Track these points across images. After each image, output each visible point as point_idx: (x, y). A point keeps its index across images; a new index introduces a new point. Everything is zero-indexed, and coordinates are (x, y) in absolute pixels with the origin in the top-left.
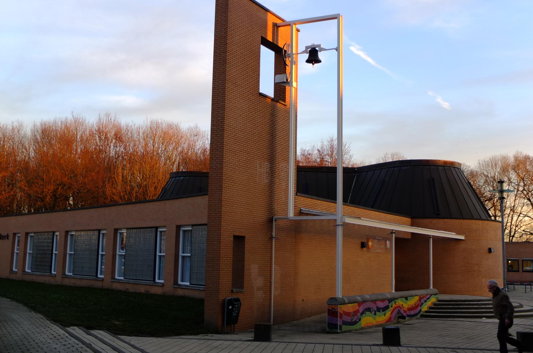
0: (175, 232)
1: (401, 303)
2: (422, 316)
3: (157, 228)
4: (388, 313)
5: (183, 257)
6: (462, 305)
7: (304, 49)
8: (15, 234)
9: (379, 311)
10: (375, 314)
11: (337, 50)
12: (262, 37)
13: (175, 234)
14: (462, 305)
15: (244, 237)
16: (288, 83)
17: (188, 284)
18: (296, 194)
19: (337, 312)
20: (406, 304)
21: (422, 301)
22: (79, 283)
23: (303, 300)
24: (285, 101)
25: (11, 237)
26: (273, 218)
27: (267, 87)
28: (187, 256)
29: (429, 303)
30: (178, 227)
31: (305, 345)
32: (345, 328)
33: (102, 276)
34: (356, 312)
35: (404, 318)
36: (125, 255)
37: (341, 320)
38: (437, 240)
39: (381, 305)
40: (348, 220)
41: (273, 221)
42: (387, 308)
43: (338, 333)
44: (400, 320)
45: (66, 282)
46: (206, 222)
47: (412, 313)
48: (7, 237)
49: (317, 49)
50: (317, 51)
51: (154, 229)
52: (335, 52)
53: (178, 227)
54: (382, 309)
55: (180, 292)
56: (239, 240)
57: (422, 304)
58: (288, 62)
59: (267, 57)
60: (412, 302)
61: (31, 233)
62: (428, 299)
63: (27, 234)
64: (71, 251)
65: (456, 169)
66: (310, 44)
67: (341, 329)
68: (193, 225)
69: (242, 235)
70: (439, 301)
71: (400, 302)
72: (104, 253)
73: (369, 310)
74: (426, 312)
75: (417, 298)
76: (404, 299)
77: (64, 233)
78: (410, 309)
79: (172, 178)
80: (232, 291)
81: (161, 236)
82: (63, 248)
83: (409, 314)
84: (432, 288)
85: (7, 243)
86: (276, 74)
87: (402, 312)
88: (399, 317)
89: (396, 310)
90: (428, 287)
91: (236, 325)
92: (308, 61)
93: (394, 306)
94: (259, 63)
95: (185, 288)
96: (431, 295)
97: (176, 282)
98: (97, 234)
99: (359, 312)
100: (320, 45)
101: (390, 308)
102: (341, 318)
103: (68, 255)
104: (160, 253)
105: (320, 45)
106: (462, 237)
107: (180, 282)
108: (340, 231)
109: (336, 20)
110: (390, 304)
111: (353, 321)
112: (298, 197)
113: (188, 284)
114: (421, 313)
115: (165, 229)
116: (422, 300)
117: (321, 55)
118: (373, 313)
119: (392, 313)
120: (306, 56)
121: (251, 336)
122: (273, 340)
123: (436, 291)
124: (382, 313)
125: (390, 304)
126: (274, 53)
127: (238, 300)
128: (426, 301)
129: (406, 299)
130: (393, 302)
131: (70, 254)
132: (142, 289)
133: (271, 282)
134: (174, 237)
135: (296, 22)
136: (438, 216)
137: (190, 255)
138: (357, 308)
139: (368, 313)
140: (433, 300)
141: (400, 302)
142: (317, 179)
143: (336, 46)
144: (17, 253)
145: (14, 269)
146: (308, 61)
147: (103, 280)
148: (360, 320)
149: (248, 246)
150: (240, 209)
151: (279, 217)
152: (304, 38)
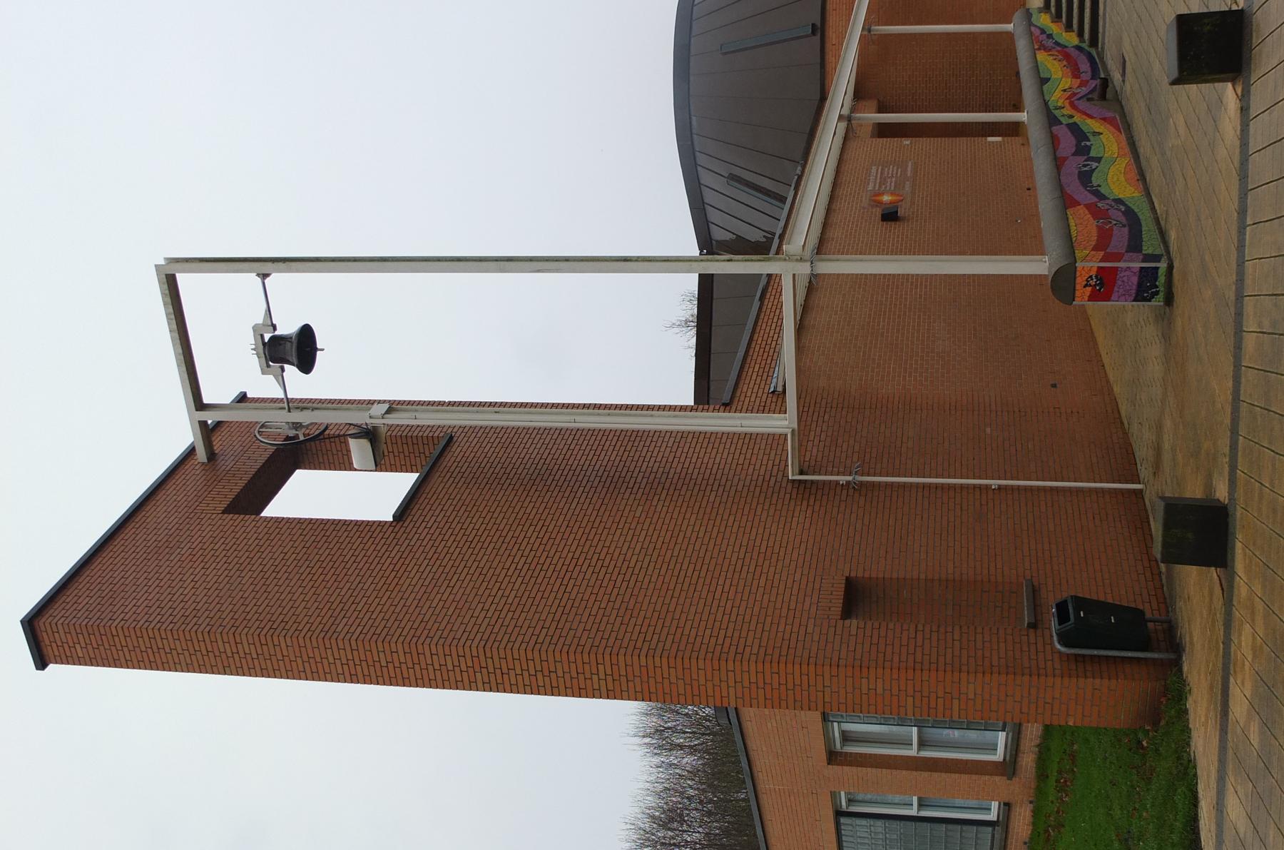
0: (846, 768)
1: (1058, 94)
3: (839, 814)
4: (1091, 125)
5: (922, 744)
7: (270, 379)
9: (1088, 148)
10: (1098, 160)
13: (854, 769)
15: (847, 579)
16: (370, 434)
18: (726, 405)
19: (1099, 268)
20: (1061, 81)
21: (1049, 43)
23: (1054, 386)
29: (1056, 29)
32: (1150, 244)
33: (995, 805)
35: (1105, 83)
37: (1127, 256)
39: (1068, 143)
42: (1075, 129)
43: (1170, 268)
44: (1109, 95)
47: (1085, 66)
49: (267, 337)
50: (273, 339)
51: (843, 820)
52: (278, 280)
55: (1028, 761)
57: (1057, 43)
59: (306, 496)
60: (1053, 66)
62: (1043, 31)
67: (1157, 258)
71: (1056, 97)
72: (915, 799)
73: (1085, 177)
74: (1080, 34)
75: (1041, 56)
76: (1045, 87)
77: (835, 769)
78: (1076, 73)
83: (1089, 74)
84: (1009, 27)
86: (351, 468)
87: (1084, 90)
88: (1103, 97)
89: (1083, 105)
90: (1010, 36)
91: (1148, 615)
94: (300, 521)
101: (1076, 119)
102: (1117, 257)
105: (255, 328)
107: (999, 756)
110: (1064, 121)
111: (1124, 221)
115: (843, 794)
116: (1042, 41)
117: (288, 327)
118: (1094, 165)
119: (1091, 117)
120: (291, 371)
122: (1222, 493)
123: (1018, 16)
126: (299, 473)
127: (1062, 607)
128: (1050, 36)
129: (1044, 81)
130: (1057, 113)
136: (819, 30)
138: (1081, 210)
139: (1095, 180)
141: (1056, 97)
146: (306, 364)
148: (1119, 201)
152: (233, 372)
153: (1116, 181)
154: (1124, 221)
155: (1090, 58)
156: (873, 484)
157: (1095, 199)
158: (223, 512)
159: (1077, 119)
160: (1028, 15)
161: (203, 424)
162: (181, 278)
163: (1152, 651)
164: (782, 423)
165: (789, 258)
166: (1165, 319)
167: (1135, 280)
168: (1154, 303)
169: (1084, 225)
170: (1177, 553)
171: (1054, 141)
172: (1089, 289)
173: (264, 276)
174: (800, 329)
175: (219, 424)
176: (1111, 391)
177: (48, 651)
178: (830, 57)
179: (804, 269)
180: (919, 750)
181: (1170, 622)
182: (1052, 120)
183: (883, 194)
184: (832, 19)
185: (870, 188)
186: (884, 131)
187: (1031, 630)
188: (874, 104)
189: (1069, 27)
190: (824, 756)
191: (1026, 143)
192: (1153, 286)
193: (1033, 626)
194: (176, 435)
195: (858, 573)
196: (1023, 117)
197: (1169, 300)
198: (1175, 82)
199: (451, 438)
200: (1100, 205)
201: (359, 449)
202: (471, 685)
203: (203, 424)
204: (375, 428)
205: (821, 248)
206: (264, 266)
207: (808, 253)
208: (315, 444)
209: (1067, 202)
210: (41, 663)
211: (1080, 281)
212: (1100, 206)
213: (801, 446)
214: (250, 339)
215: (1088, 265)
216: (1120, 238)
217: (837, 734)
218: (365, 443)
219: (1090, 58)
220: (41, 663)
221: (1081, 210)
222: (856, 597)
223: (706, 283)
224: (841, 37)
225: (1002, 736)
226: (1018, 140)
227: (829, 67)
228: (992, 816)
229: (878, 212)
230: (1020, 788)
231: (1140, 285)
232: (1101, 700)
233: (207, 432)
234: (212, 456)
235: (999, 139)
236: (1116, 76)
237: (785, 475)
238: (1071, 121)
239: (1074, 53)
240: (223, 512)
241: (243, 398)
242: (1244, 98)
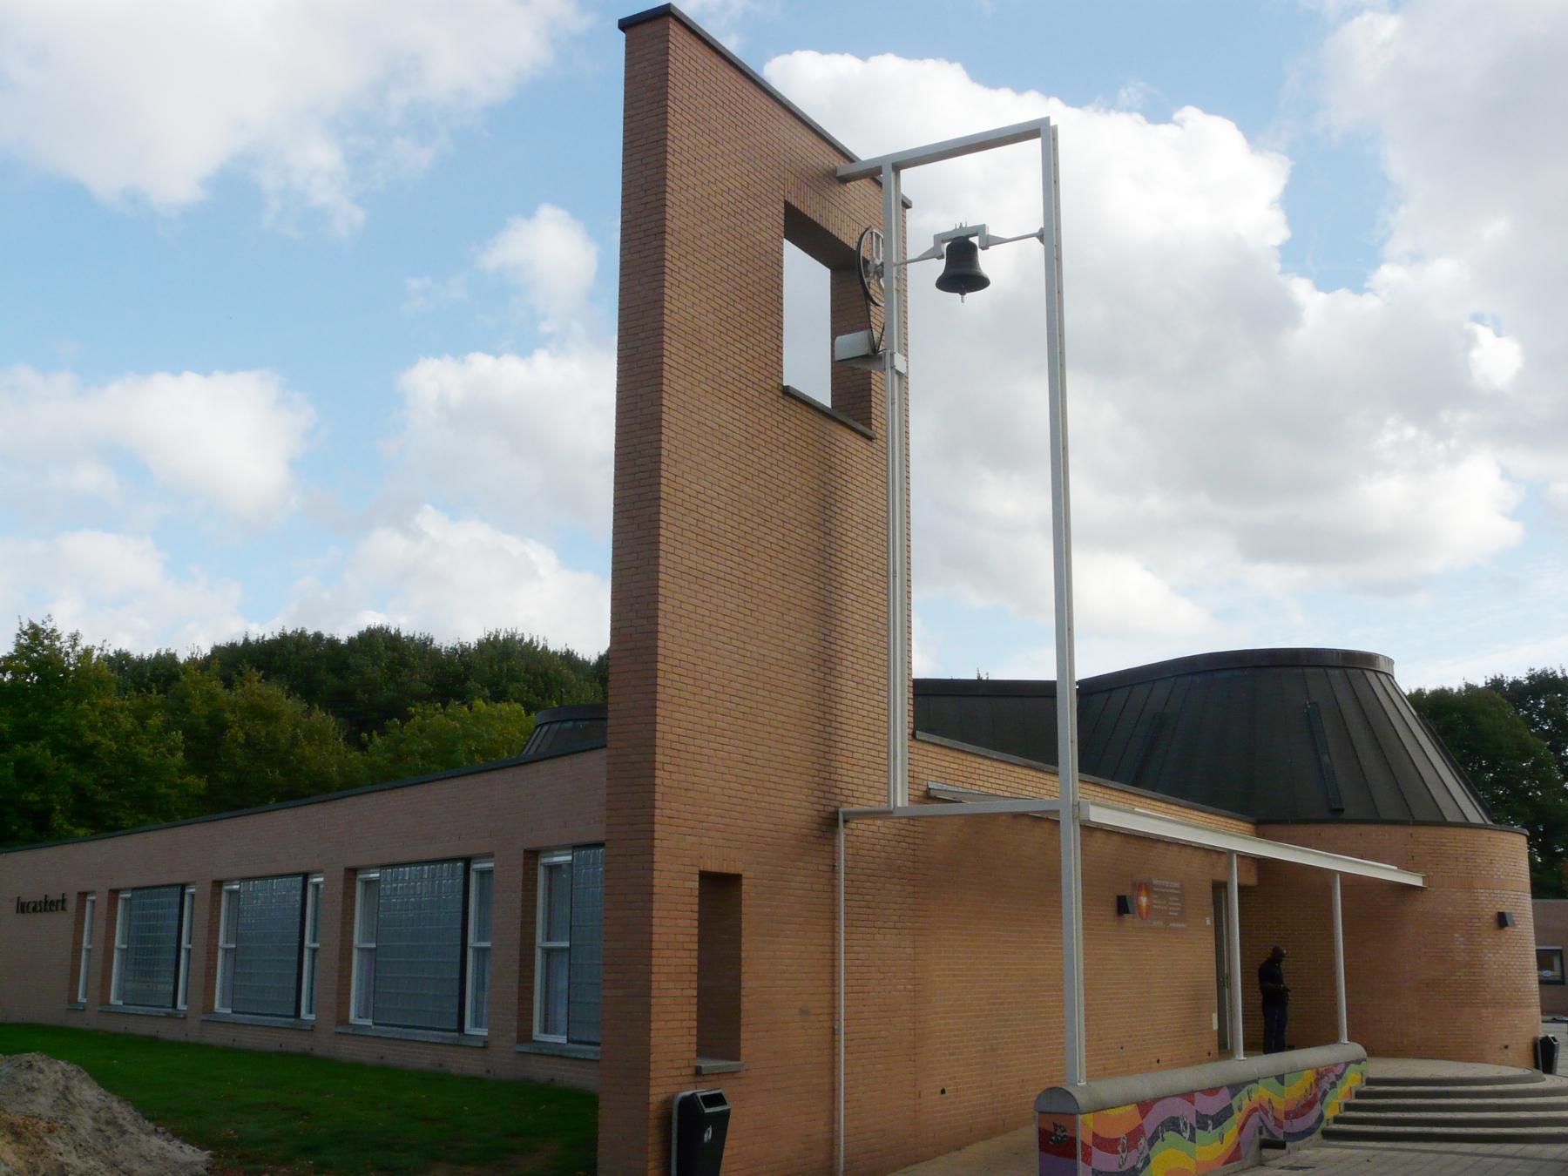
2: (1329, 1135)
3: (467, 861)
4: (1231, 1130)
5: (548, 952)
8: (83, 895)
9: (1204, 1127)
10: (1192, 1139)
12: (788, 207)
15: (740, 876)
16: (874, 355)
17: (563, 1039)
18: (914, 735)
20: (1283, 1098)
21: (1325, 1085)
22: (249, 1039)
23: (943, 1092)
24: (869, 425)
25: (72, 905)
26: (837, 813)
27: (808, 365)
28: (562, 949)
30: (532, 855)
33: (483, 1032)
34: (1135, 1135)
36: (569, 949)
38: (1353, 884)
40: (1099, 815)
41: (837, 825)
42: (1227, 1112)
44: (1267, 1153)
45: (348, 1050)
46: (602, 838)
47: (1298, 1125)
49: (975, 240)
50: (973, 247)
52: (1036, 247)
54: (1212, 1118)
55: (542, 1070)
56: (719, 888)
57: (1325, 1094)
58: (873, 290)
60: (1296, 1090)
62: (1339, 1077)
63: (114, 893)
64: (480, 938)
65: (1382, 677)
66: (950, 228)
68: (576, 847)
69: (732, 870)
70: (1370, 1082)
72: (487, 944)
73: (1173, 1124)
74: (1337, 1120)
75: (1310, 1076)
77: (519, 860)
78: (1292, 1115)
79: (542, 725)
81: (550, 880)
86: (836, 332)
87: (1271, 1124)
88: (1265, 1145)
89: (1254, 1120)
93: (1246, 1105)
95: (557, 1054)
96: (1347, 1064)
97: (525, 1035)
98: (299, 885)
99: (1143, 1133)
100: (983, 227)
103: (355, 952)
104: (549, 939)
105: (983, 227)
106: (1415, 880)
109: (1035, 145)
112: (917, 745)
113: (563, 1039)
114: (1323, 1126)
117: (987, 261)
118: (1187, 1135)
120: (939, 267)
123: (1357, 1050)
124: (1212, 1133)
125: (1235, 1103)
126: (828, 272)
127: (717, 1099)
128: (1333, 1085)
130: (1243, 1093)
132: (424, 1059)
133: (834, 1032)
134: (519, 889)
135: (900, 164)
136: (1336, 815)
137: (566, 944)
140: (1353, 1080)
143: (1037, 224)
144: (189, 951)
145: (81, 999)
147: (312, 1029)
148: (1147, 1161)
149: (1372, 1075)
150: (714, 785)
151: (857, 808)
152: (936, 205)
154: (1124, 1168)
157: (1149, 1135)
158: (786, 203)
159: (1238, 1117)
161: (878, 171)
162: (1037, 142)
163: (1479, 1058)
169: (1120, 1122)
171: (1212, 1091)
172: (1052, 1129)
173: (1041, 236)
177: (638, 30)
180: (543, 949)
182: (1235, 1088)
183: (1148, 895)
185: (1155, 882)
186: (1219, 888)
187: (691, 1071)
188: (1252, 880)
191: (1211, 1058)
193: (698, 1071)
194: (865, 149)
195: (746, 886)
199: (870, 438)
200: (1143, 1140)
201: (853, 343)
203: (878, 171)
204: (880, 358)
206: (1049, 235)
208: (857, 287)
209: (1145, 1107)
210: (625, 25)
214: (972, 222)
217: (556, 859)
220: (625, 25)
223: (1045, 691)
226: (1215, 1049)
228: (469, 1028)
229: (1126, 891)
235: (1215, 1027)
238: (1235, 1108)
239: (1314, 1114)
240: (786, 203)
241: (906, 205)
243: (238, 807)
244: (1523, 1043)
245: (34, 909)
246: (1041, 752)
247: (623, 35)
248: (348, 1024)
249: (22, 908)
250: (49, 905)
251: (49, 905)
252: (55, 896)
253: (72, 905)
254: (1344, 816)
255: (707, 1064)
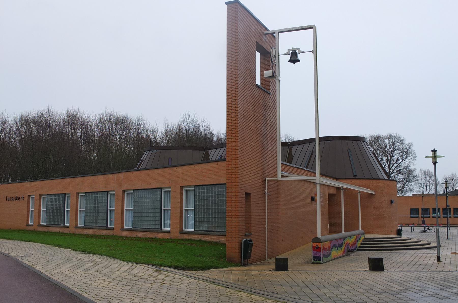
0: (179, 191)
2: (359, 250)
6: (382, 241)
11: (313, 53)
14: (382, 241)
20: (351, 241)
24: (269, 90)
25: (26, 198)
28: (113, 210)
29: (360, 241)
31: (431, 270)
39: (340, 242)
43: (321, 263)
45: (79, 231)
48: (23, 198)
49: (297, 51)
52: (312, 55)
53: (182, 187)
55: (186, 237)
61: (82, 193)
73: (334, 246)
74: (360, 247)
75: (355, 237)
80: (245, 235)
82: (75, 206)
84: (360, 229)
85: (23, 204)
88: (348, 251)
90: (358, 229)
92: (290, 61)
93: (346, 243)
100: (299, 49)
103: (125, 211)
105: (299, 49)
108: (318, 187)
109: (312, 30)
116: (358, 238)
117: (300, 56)
120: (289, 57)
121: (273, 267)
123: (363, 231)
131: (32, 211)
136: (355, 177)
141: (348, 240)
142: (293, 151)
146: (290, 61)
152: (285, 44)
153: (335, 253)
155: (355, 249)
156: (265, 198)
159: (344, 245)
160: (363, 234)
164: (279, 177)
165: (319, 178)
166: (308, 262)
167: (318, 256)
168: (313, 260)
169: (327, 245)
170: (278, 261)
174: (304, 180)
175: (275, 37)
176: (282, 254)
178: (348, 180)
179: (317, 182)
181: (247, 264)
182: (344, 238)
184: (358, 181)
189: (361, 244)
190: (183, 185)
192: (317, 260)
193: (245, 235)
194: (271, 27)
196: (343, 232)
197: (313, 263)
198: (369, 259)
202: (228, 109)
205: (322, 185)
206: (315, 52)
207: (321, 182)
208: (269, 59)
210: (227, 3)
211: (317, 244)
212: (330, 249)
213: (274, 181)
215: (321, 245)
216: (325, 253)
218: (271, 75)
219: (355, 249)
220: (227, 3)
221: (329, 245)
222: (248, 195)
224: (353, 184)
225: (193, 230)
227: (345, 180)
229: (313, 196)
230: (175, 234)
231: (317, 257)
232: (233, 250)
233: (272, 34)
234: (266, 34)
236: (353, 254)
237: (266, 177)
242: (367, 271)
243: (84, 174)
244: (395, 231)
245: (13, 200)
246: (309, 166)
247: (226, 6)
248: (106, 228)
249: (8, 199)
250: (18, 199)
251: (18, 199)
252: (20, 196)
253: (26, 198)
254: (357, 177)
255: (441, 211)
